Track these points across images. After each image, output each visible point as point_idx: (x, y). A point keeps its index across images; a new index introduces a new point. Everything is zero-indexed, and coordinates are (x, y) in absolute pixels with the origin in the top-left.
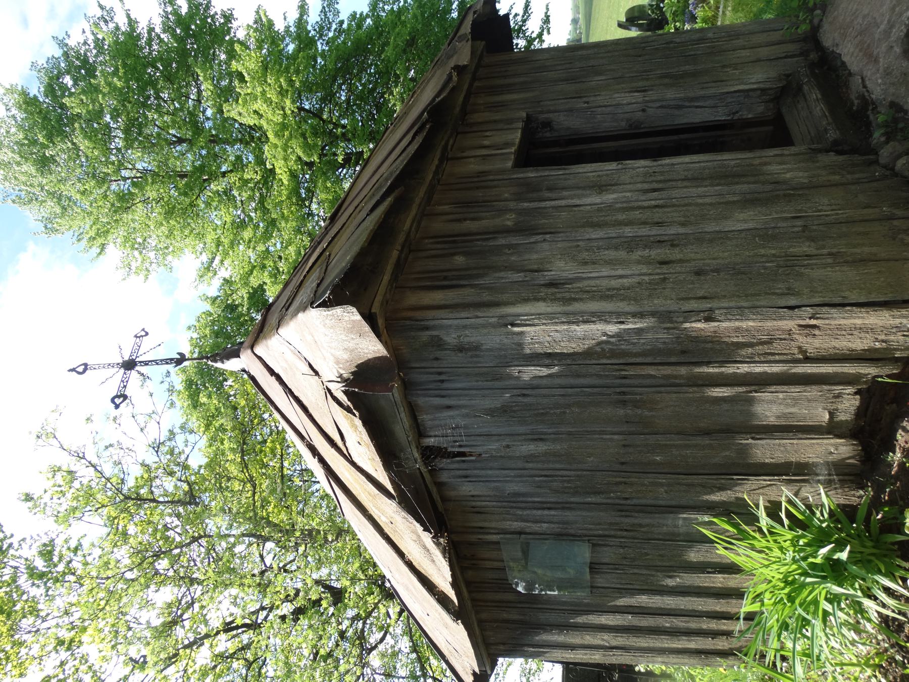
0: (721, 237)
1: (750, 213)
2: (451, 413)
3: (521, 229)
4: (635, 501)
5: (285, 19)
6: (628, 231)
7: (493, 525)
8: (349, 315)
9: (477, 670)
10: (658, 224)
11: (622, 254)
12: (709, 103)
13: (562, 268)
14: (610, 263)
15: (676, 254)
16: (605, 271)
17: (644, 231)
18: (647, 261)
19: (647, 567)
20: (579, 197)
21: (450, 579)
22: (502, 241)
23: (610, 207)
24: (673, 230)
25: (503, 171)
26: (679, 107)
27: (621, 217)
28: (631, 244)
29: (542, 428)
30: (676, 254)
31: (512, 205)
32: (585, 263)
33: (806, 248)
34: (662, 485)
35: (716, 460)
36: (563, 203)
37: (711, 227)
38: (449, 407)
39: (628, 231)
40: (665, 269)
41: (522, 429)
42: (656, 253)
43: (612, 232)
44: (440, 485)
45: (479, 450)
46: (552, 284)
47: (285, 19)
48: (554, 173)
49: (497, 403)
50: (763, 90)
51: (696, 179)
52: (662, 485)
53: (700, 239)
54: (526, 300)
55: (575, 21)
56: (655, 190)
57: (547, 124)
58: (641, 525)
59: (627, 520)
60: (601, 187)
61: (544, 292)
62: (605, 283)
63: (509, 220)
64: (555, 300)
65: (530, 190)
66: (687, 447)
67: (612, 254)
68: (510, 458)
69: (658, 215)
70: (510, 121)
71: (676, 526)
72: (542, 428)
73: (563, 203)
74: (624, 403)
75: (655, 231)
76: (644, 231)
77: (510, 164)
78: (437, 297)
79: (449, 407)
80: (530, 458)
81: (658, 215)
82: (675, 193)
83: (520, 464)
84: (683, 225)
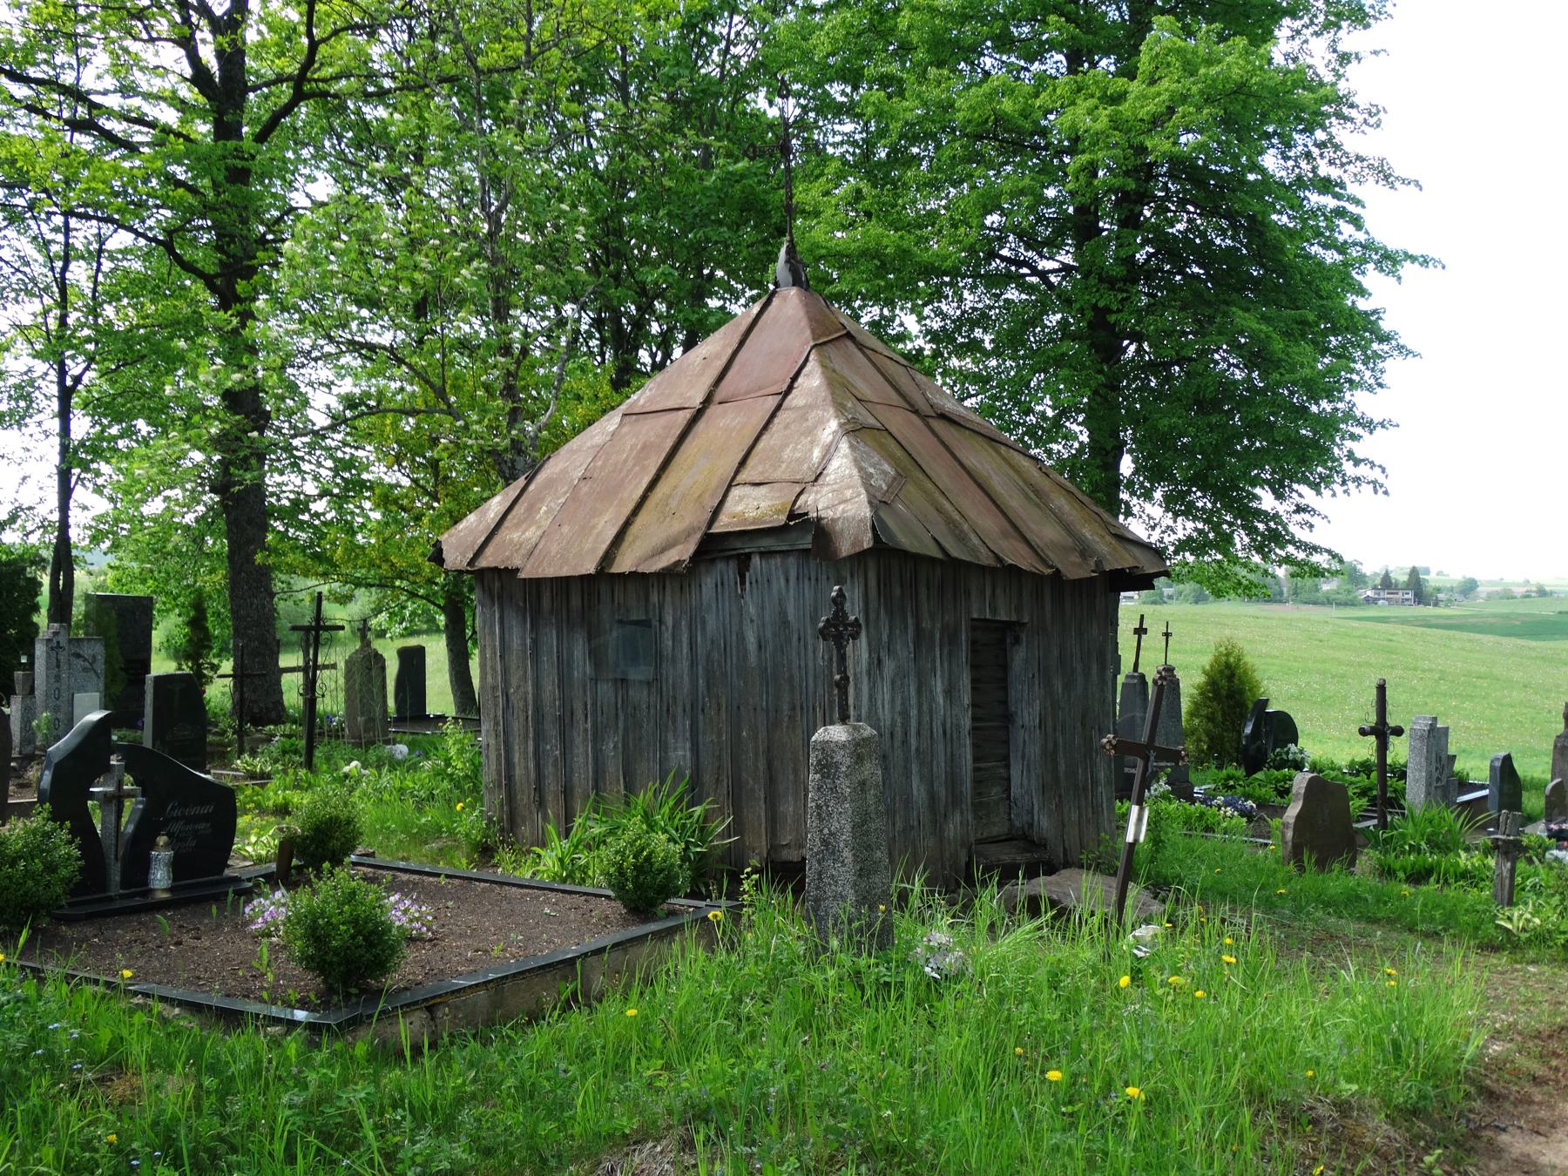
0: (908, 776)
1: (924, 794)
2: (782, 581)
3: (919, 631)
4: (701, 717)
5: (1375, 53)
6: (914, 713)
7: (668, 598)
8: (867, 542)
9: (522, 575)
10: (918, 733)
11: (898, 708)
12: (1025, 782)
13: (889, 667)
14: (893, 701)
15: (897, 744)
16: (887, 697)
17: (914, 723)
18: (893, 724)
19: (626, 729)
20: (942, 677)
21: (640, 570)
22: (910, 621)
23: (933, 699)
24: (913, 742)
25: (969, 612)
26: (1023, 757)
27: (925, 707)
28: (905, 714)
29: (770, 648)
30: (897, 744)
31: (938, 625)
32: (893, 683)
33: (899, 825)
34: (719, 735)
35: (744, 775)
36: (938, 664)
37: (915, 768)
38: (787, 581)
39: (914, 713)
40: (888, 736)
41: (769, 634)
42: (898, 730)
43: (914, 701)
44: (713, 561)
45: (747, 597)
46: (879, 661)
47: (1375, 53)
48: (964, 654)
49: (791, 617)
50: (1031, 825)
51: (952, 760)
52: (719, 735)
53: (907, 760)
54: (869, 644)
55: (1469, 587)
56: (945, 732)
57: (1017, 641)
58: (674, 722)
59: (680, 710)
60: (950, 692)
61: (875, 656)
62: (879, 697)
63: (927, 624)
64: (870, 664)
65: (951, 637)
66: (756, 754)
67: (899, 702)
68: (741, 622)
69: (925, 733)
70: (1019, 609)
71: (675, 749)
72: (770, 648)
73: (938, 664)
74: (793, 708)
75: (913, 731)
76: (914, 723)
77: (975, 616)
78: (873, 583)
79: (787, 581)
80: (741, 638)
81: (925, 733)
82: (941, 747)
83: (735, 628)
84: (917, 749)
